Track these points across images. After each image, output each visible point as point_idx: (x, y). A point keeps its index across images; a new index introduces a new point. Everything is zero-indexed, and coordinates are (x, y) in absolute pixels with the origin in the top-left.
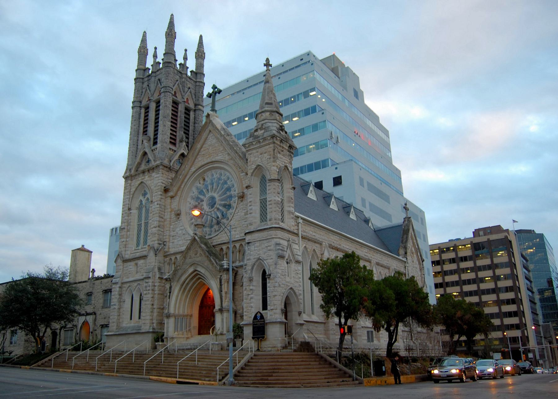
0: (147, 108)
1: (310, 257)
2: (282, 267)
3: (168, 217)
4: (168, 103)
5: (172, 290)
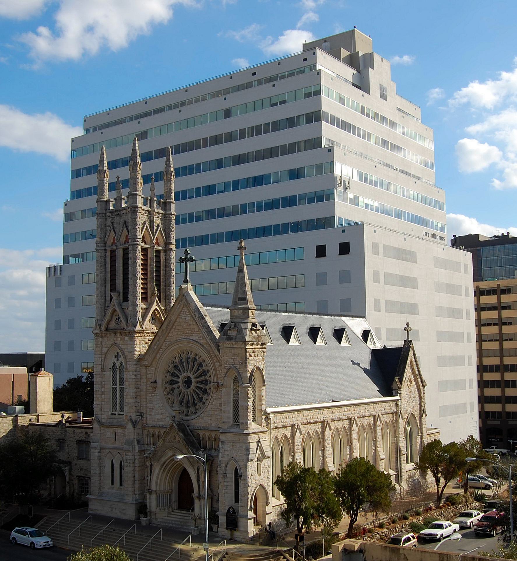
3: (144, 387)
5: (153, 468)
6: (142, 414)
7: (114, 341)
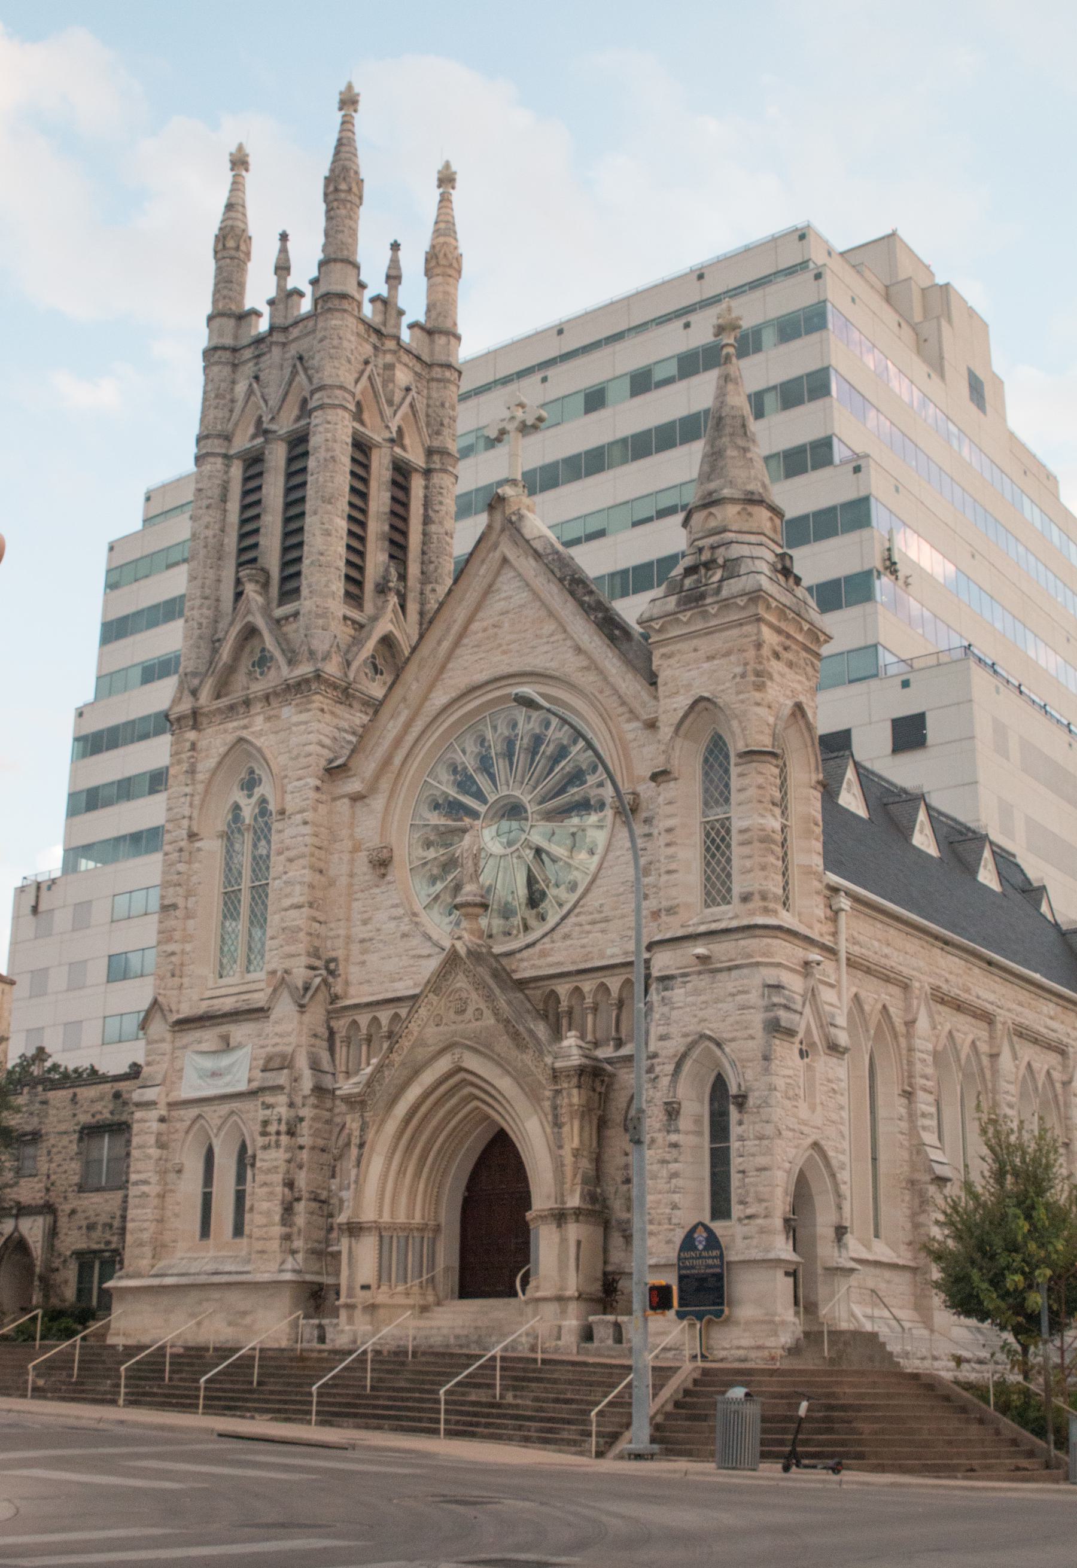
0: (254, 462)
1: (872, 1032)
2: (788, 1068)
3: (345, 869)
4: (337, 447)
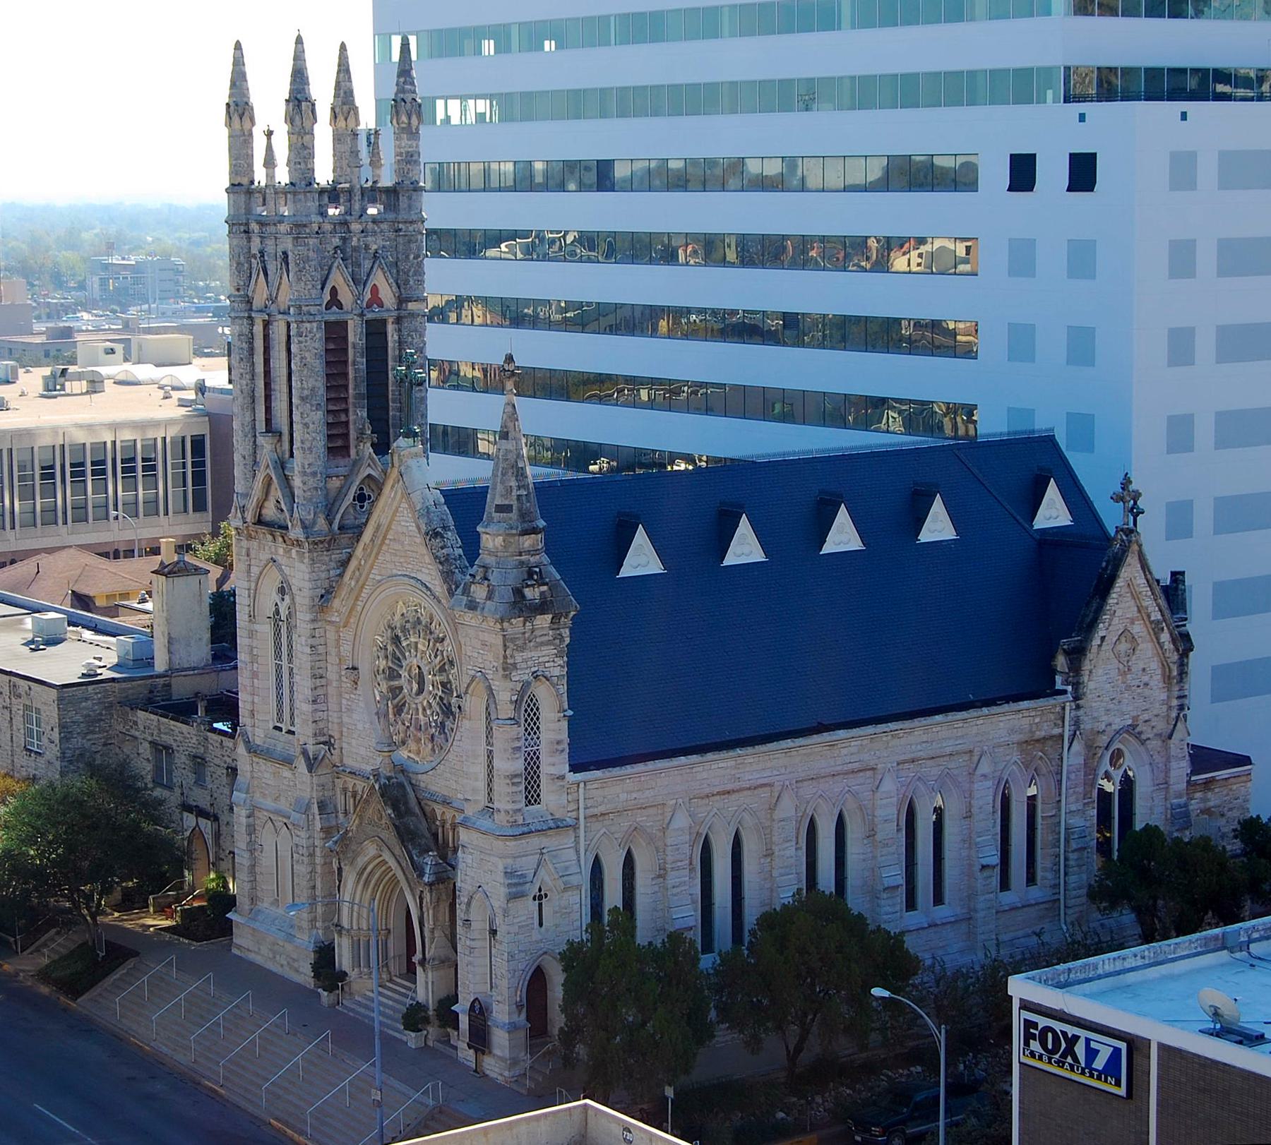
6: (332, 740)
7: (271, 553)
